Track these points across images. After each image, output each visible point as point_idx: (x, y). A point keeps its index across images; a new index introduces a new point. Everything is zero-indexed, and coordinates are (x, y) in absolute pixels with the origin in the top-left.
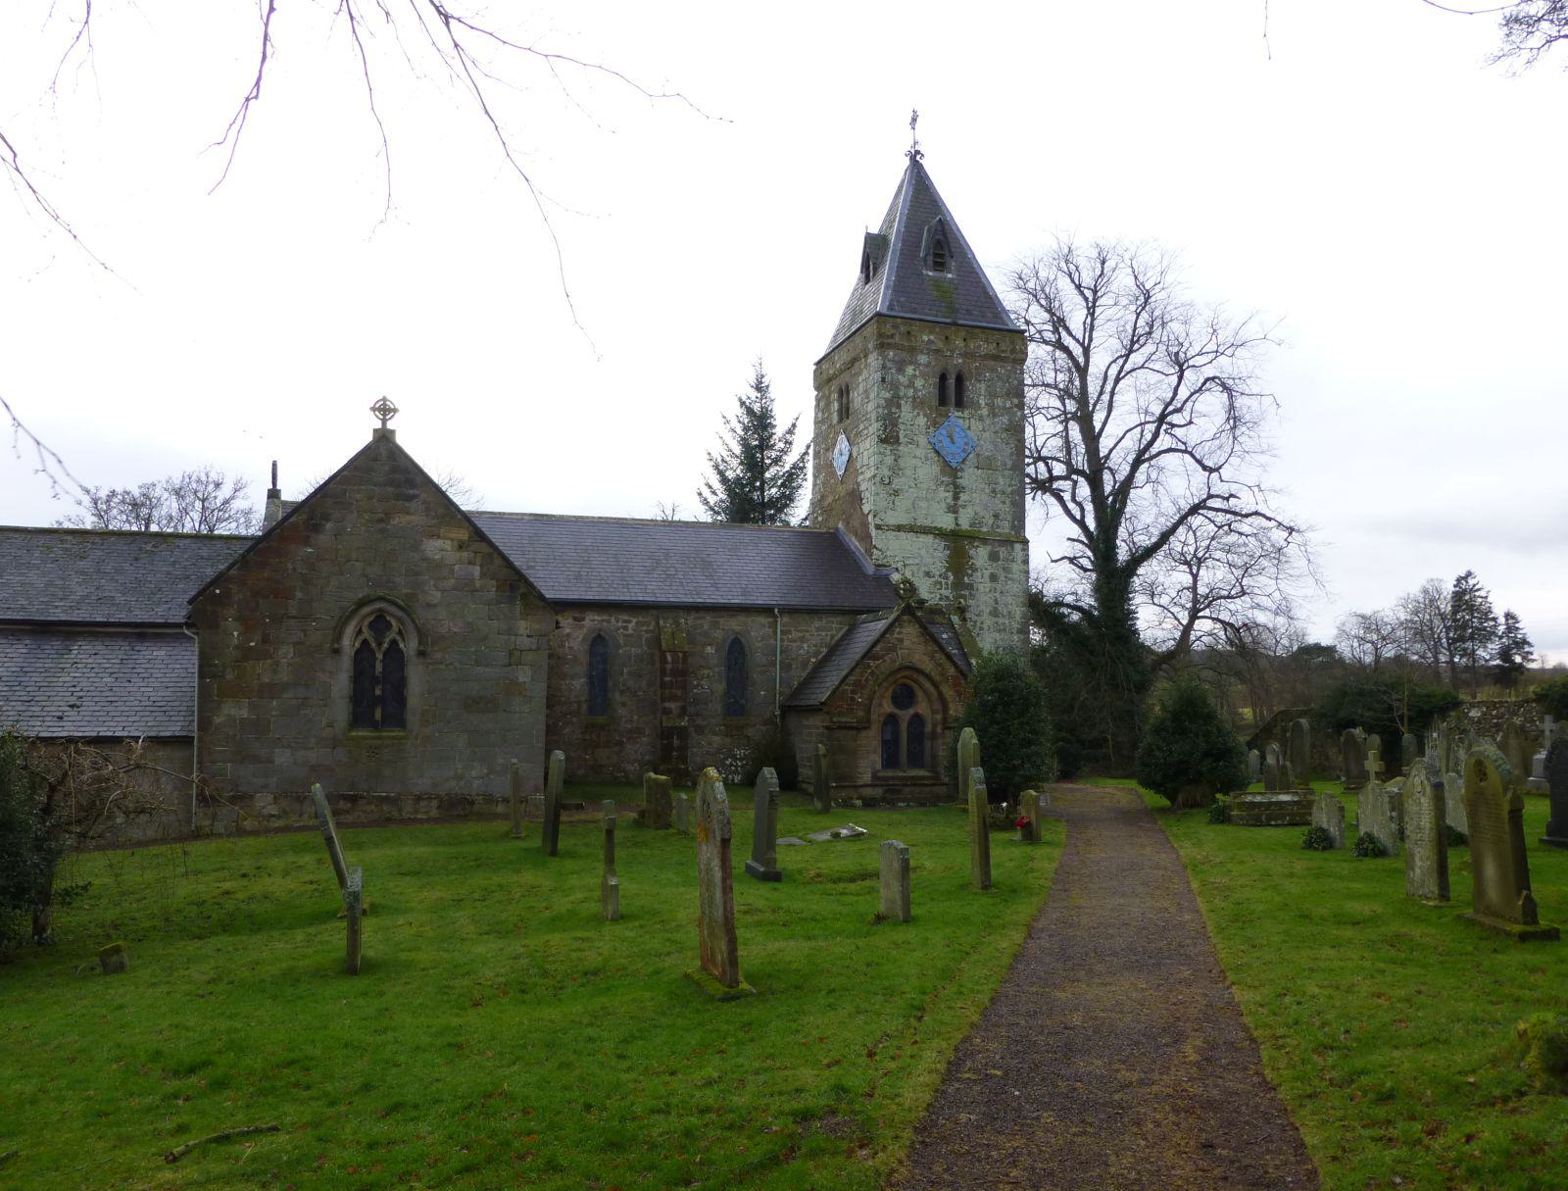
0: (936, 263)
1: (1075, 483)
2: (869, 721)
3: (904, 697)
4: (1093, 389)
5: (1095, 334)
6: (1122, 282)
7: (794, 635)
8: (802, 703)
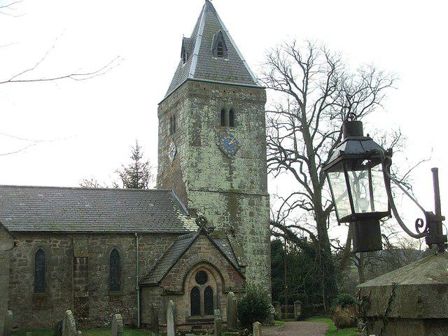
0: (219, 54)
1: (302, 163)
2: (183, 290)
3: (202, 278)
4: (309, 116)
5: (308, 86)
6: (320, 62)
7: (146, 246)
8: (151, 282)
